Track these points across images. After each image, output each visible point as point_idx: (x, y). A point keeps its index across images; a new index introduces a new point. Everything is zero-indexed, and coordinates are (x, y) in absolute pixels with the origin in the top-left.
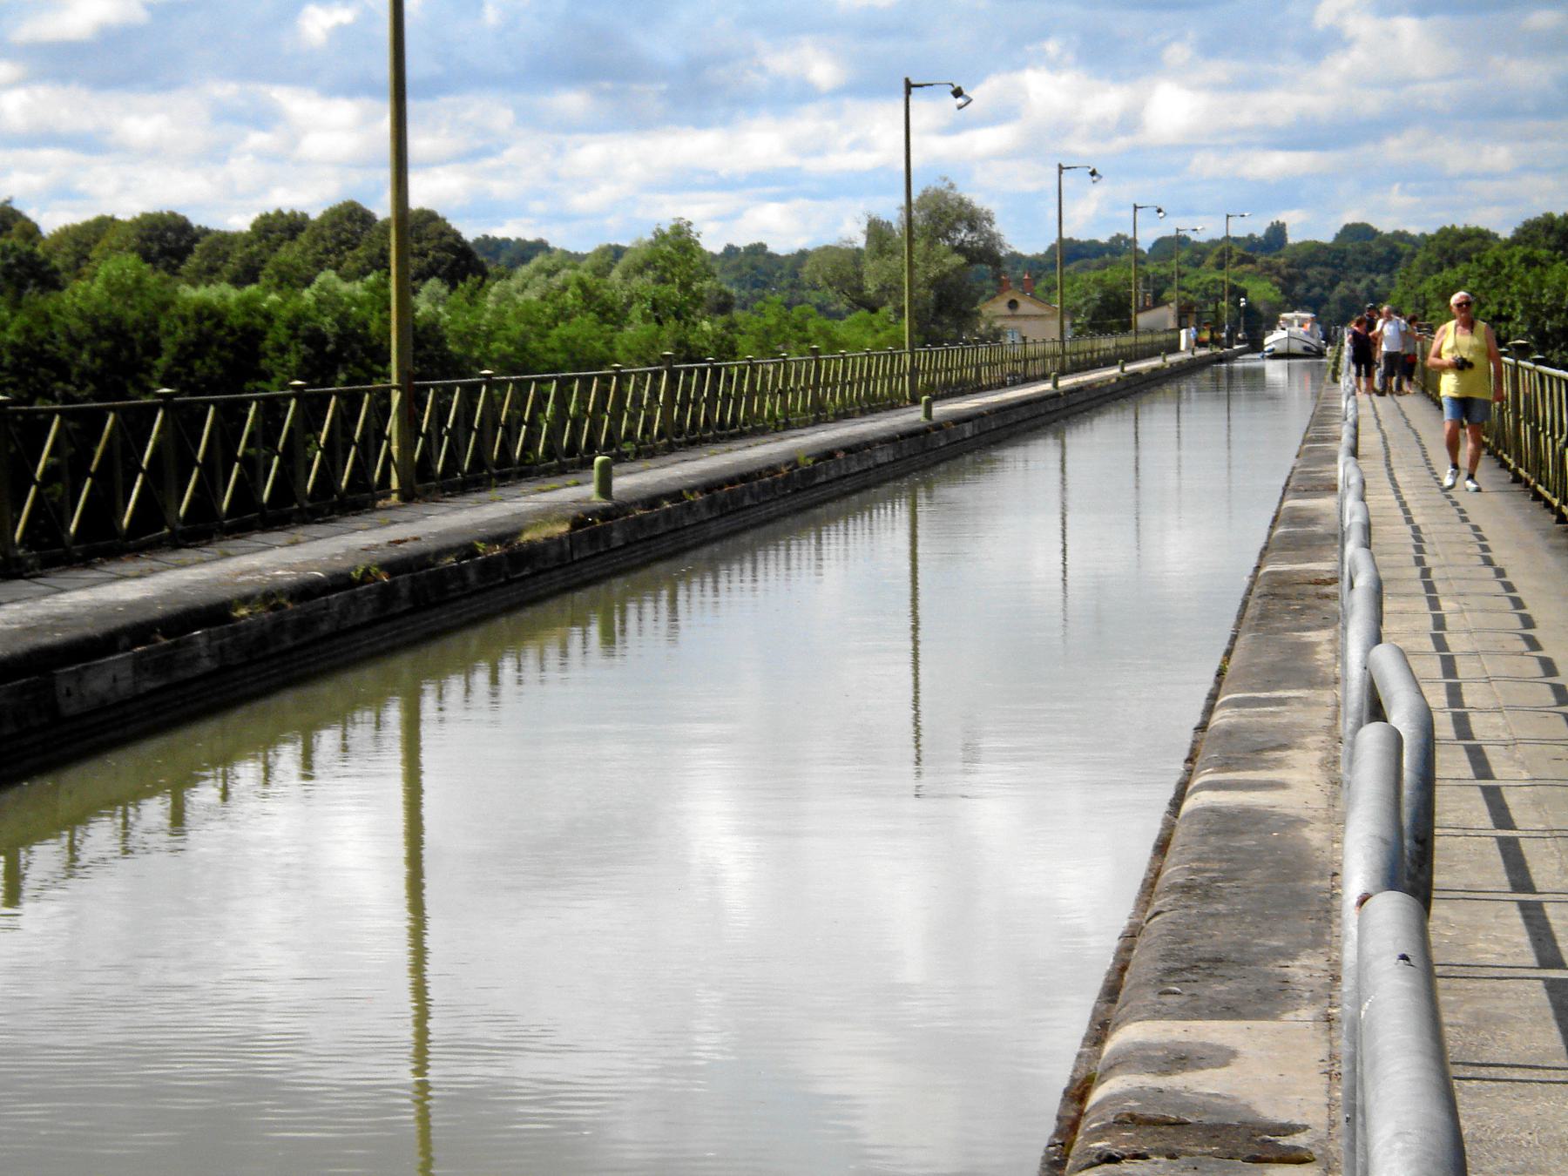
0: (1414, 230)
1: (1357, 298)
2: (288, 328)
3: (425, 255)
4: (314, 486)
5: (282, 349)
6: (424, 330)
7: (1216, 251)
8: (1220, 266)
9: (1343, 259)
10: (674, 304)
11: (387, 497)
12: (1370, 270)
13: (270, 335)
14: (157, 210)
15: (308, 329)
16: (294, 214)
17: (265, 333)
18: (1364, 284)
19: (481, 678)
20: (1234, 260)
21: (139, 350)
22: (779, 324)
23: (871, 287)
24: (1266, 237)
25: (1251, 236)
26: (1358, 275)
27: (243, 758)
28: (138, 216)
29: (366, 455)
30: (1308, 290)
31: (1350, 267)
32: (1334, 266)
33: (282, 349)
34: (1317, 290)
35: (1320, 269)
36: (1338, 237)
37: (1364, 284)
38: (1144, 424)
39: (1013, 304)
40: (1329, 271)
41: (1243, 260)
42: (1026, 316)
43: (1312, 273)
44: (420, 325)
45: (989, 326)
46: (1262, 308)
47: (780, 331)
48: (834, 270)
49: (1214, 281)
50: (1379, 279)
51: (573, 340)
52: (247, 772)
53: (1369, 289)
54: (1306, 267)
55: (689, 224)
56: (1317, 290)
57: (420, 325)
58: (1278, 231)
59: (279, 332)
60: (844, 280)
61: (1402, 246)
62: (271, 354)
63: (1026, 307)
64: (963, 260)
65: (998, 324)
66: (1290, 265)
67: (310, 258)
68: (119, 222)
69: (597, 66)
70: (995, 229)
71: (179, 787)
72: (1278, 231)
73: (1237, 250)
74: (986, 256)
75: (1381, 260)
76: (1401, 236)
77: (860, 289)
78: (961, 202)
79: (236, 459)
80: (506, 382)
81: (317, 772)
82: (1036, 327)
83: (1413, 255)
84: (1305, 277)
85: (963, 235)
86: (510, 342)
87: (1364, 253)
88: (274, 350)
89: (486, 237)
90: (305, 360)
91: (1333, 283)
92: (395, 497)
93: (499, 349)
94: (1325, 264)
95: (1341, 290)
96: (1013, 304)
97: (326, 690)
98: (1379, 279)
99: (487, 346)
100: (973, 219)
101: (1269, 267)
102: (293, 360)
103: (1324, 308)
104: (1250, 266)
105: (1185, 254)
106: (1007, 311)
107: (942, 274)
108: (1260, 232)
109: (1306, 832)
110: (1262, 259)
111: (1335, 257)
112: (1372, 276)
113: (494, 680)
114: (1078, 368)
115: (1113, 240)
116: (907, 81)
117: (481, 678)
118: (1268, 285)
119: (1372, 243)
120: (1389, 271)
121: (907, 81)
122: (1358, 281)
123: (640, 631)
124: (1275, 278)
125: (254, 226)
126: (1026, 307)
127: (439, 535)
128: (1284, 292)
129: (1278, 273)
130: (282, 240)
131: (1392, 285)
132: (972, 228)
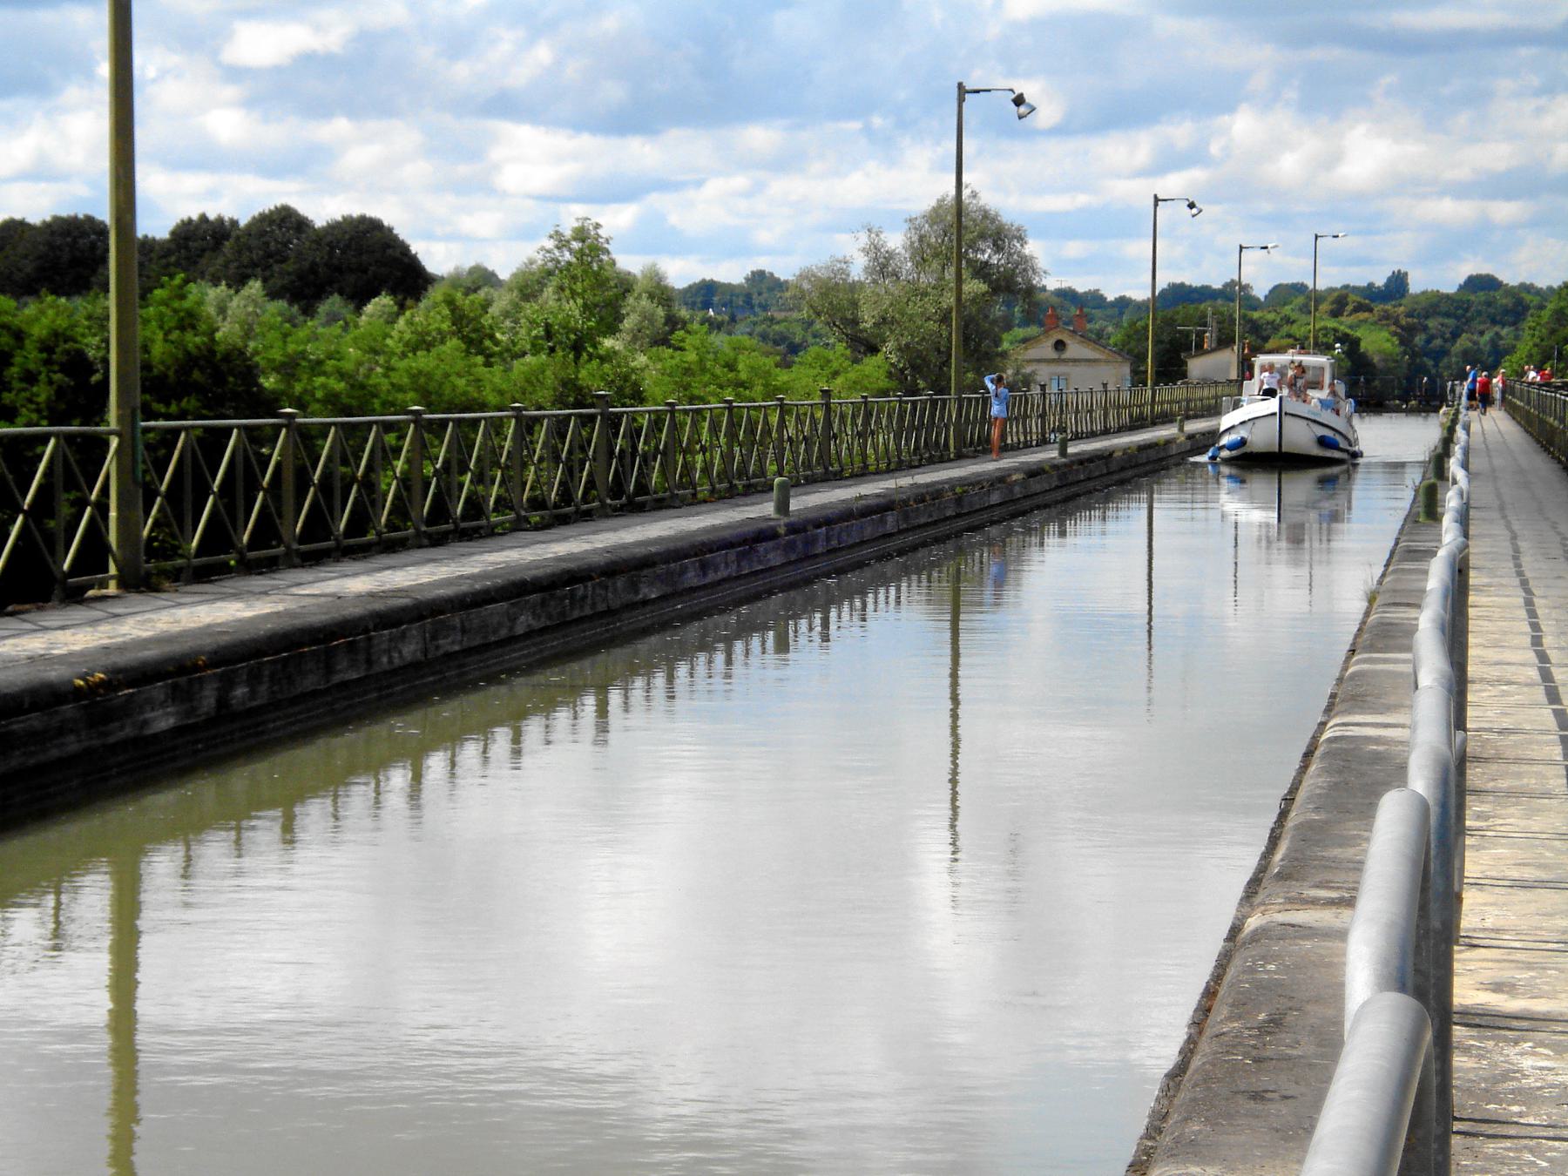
0: (1542, 283)
1: (1479, 351)
2: (41, 351)
3: (365, 271)
4: (464, 508)
5: (30, 378)
6: (227, 357)
7: (1330, 299)
8: (1335, 314)
9: (1467, 310)
10: (575, 331)
11: (103, 584)
12: (1494, 322)
13: (18, 360)
14: (72, 214)
15: (67, 352)
16: (220, 220)
17: (12, 356)
18: (1487, 337)
19: (659, 680)
20: (1349, 308)
21: (43, 377)
22: (701, 361)
23: (868, 321)
24: (1387, 285)
25: (1371, 285)
26: (1482, 327)
27: (502, 725)
28: (48, 219)
29: (231, 509)
30: (1428, 341)
31: (1472, 319)
32: (1457, 318)
33: (30, 378)
34: (1438, 342)
35: (1441, 320)
36: (1461, 287)
37: (1487, 337)
38: (196, 849)
39: (1060, 345)
40: (1451, 322)
41: (1359, 308)
42: (1075, 361)
43: (1432, 323)
44: (221, 349)
45: (1017, 373)
46: (1376, 359)
47: (704, 370)
48: (824, 295)
49: (1325, 328)
50: (1504, 332)
51: (429, 376)
52: (470, 752)
53: (1493, 343)
54: (1427, 317)
55: (598, 226)
56: (1438, 342)
57: (221, 349)
58: (1398, 283)
59: (30, 356)
60: (834, 310)
61: (1528, 298)
62: (16, 385)
63: (1075, 349)
64: (984, 287)
65: (1028, 370)
66: (1409, 315)
67: (231, 271)
68: (28, 225)
69: (686, 88)
70: (1027, 250)
71: (416, 760)
72: (1398, 283)
73: (1352, 297)
74: (1012, 286)
75: (1506, 312)
76: (1527, 288)
77: (855, 322)
78: (986, 214)
79: (20, 510)
80: (443, 424)
81: (300, 836)
82: (1091, 377)
83: (1541, 307)
84: (1425, 328)
85: (987, 254)
86: (342, 375)
87: (1489, 304)
88: (21, 380)
89: (203, 218)
90: (60, 392)
91: (1455, 335)
92: (113, 584)
93: (324, 386)
94: (1448, 315)
95: (1463, 342)
96: (1060, 345)
97: (447, 711)
98: (1504, 332)
99: (310, 379)
100: (1000, 236)
101: (1386, 316)
102: (43, 393)
103: (1446, 360)
104: (1366, 315)
105: (1300, 300)
106: (1054, 355)
107: (967, 308)
108: (1380, 281)
109: (1420, 791)
110: (1379, 308)
111: (1457, 308)
112: (1497, 328)
113: (517, 739)
114: (1138, 424)
115: (1226, 285)
116: (960, 85)
117: (659, 680)
118: (1385, 334)
119: (1498, 295)
120: (1514, 324)
121: (960, 85)
122: (1482, 333)
123: (626, 707)
124: (1393, 328)
125: (173, 233)
126: (1075, 349)
127: (607, 550)
128: (1402, 343)
129: (1396, 323)
130: (203, 250)
131: (1517, 338)
132: (998, 248)
